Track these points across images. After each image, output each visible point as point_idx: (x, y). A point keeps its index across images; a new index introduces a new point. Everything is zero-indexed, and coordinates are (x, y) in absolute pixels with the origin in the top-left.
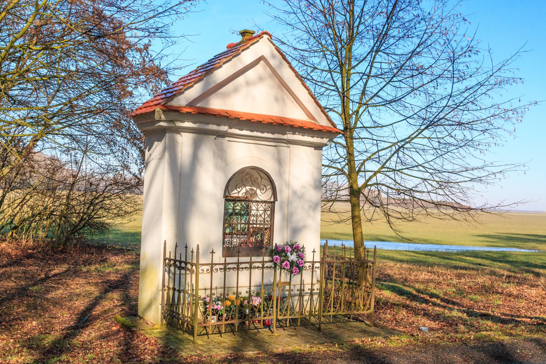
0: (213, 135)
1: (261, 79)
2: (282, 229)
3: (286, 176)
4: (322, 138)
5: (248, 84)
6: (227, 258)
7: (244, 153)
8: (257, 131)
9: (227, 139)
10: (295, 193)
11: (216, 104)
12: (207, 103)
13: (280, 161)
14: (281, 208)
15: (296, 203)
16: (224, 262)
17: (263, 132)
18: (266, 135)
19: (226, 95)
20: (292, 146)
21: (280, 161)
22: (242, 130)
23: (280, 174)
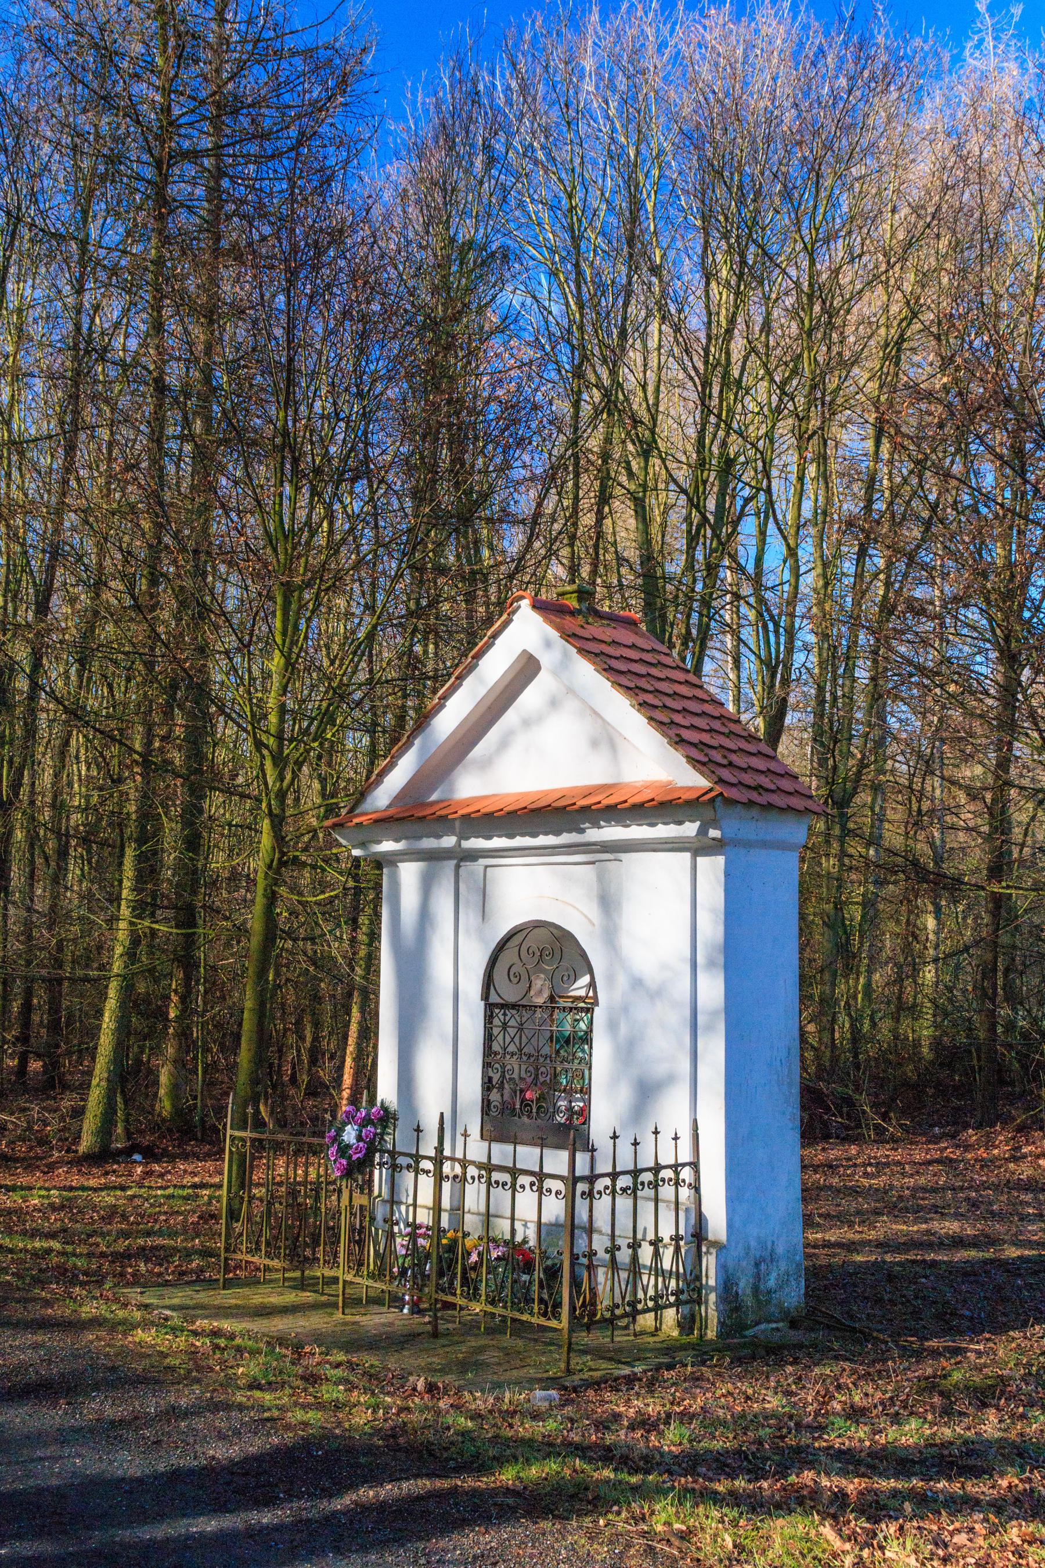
0: (450, 858)
1: (554, 703)
2: (614, 1081)
3: (627, 944)
4: (680, 823)
5: (527, 723)
6: (494, 1145)
7: (531, 888)
8: (523, 835)
9: (483, 862)
10: (637, 983)
11: (470, 786)
12: (451, 790)
13: (608, 902)
14: (613, 1026)
15: (642, 1012)
16: (610, 1170)
17: (534, 835)
18: (543, 840)
19: (486, 764)
20: (623, 856)
21: (608, 902)
22: (489, 838)
23: (610, 935)
